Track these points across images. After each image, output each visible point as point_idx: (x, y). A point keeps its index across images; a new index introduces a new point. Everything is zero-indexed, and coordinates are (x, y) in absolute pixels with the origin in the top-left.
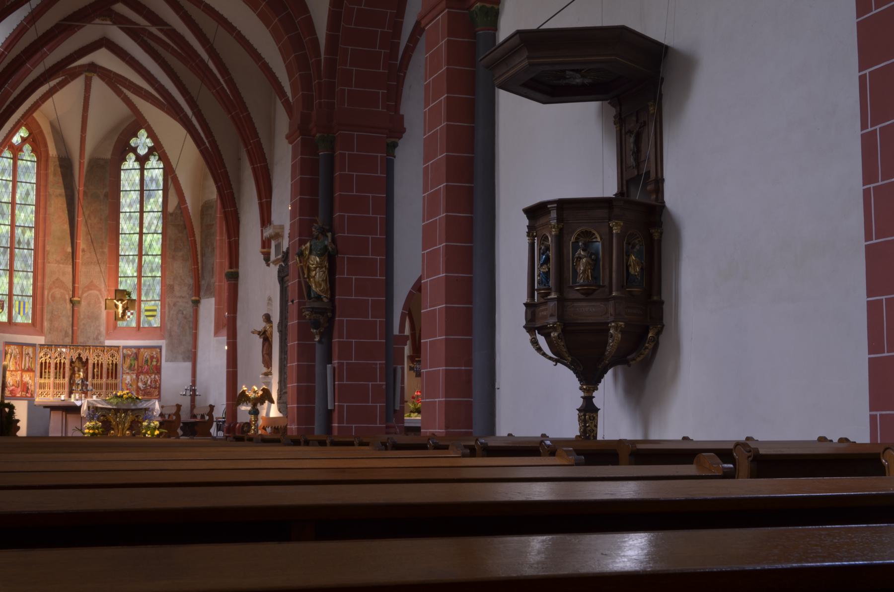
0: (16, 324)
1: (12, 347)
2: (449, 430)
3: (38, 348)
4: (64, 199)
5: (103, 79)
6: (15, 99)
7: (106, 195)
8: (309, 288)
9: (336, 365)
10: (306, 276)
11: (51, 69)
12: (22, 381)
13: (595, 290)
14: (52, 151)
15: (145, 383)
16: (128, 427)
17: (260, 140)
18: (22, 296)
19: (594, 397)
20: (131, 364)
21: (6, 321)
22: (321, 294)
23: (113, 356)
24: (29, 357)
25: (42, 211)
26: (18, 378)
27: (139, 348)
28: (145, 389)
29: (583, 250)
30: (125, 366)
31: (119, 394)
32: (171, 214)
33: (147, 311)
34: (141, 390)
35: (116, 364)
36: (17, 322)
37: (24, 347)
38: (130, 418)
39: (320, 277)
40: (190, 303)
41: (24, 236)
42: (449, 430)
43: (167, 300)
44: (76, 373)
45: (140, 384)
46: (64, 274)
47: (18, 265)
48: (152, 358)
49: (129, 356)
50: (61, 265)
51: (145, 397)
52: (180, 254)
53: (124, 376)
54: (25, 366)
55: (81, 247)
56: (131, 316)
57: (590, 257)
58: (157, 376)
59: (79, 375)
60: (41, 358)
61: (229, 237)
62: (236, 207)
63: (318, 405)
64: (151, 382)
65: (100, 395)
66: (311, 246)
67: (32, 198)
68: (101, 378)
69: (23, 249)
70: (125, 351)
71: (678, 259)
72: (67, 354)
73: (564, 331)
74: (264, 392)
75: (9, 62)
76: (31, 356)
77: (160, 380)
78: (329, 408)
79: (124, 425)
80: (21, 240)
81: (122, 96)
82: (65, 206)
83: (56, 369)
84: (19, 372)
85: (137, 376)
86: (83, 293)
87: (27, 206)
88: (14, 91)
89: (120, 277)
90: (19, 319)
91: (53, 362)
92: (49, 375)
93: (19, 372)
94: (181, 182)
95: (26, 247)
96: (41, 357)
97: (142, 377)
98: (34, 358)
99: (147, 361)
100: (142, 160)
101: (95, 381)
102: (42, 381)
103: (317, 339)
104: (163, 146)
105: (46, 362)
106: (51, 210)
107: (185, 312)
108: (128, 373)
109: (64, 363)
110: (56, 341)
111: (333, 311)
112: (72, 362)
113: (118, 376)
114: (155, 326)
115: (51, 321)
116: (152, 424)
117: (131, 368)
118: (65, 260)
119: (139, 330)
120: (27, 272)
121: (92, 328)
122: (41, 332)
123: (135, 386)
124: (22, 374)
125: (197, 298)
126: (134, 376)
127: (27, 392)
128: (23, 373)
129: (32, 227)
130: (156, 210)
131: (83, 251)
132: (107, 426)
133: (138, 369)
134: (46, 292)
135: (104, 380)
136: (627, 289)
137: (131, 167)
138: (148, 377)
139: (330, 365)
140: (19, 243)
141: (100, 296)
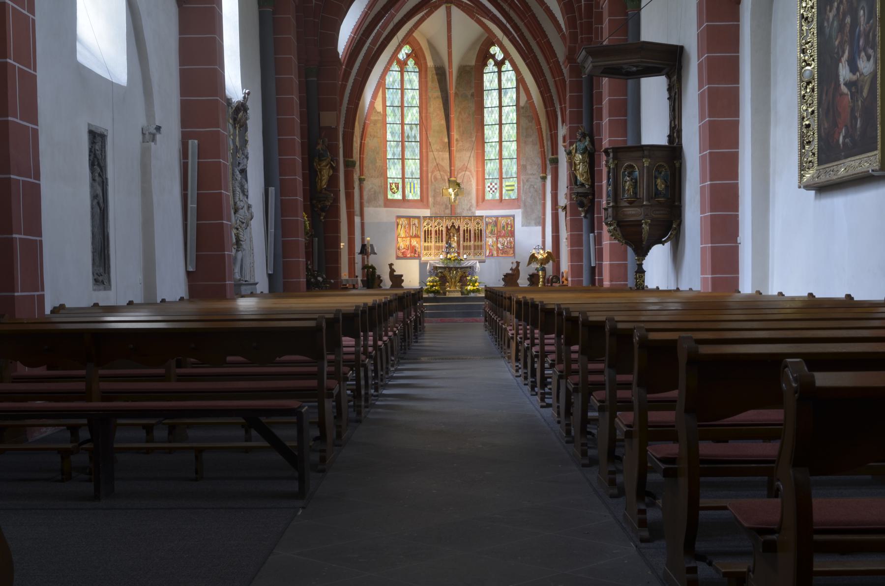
0: (409, 201)
1: (402, 219)
2: (613, 283)
3: (422, 221)
4: (441, 100)
5: (459, 8)
6: (387, 36)
7: (472, 95)
8: (576, 177)
9: (596, 234)
10: (573, 169)
11: (408, 13)
12: (411, 245)
13: (634, 201)
14: (430, 63)
15: (503, 245)
16: (459, 280)
17: (558, 60)
18: (412, 178)
19: (504, 275)
20: (492, 230)
21: (401, 199)
22: (583, 182)
23: (478, 223)
24: (416, 226)
25: (424, 111)
26: (408, 243)
27: (497, 217)
28: (503, 249)
29: (629, 177)
30: (488, 231)
31: (448, 257)
32: (523, 108)
33: (507, 186)
34: (500, 250)
35: (481, 230)
36: (409, 199)
37: (411, 219)
38: (460, 274)
39: (583, 170)
40: (539, 179)
41: (411, 131)
42: (613, 283)
43: (522, 177)
44: (452, 237)
45: (499, 245)
46: (443, 159)
47: (408, 154)
48: (507, 224)
49: (490, 223)
50: (440, 153)
51: (503, 255)
52: (531, 140)
53: (487, 240)
54: (413, 234)
55: (455, 138)
56: (495, 191)
57: (632, 180)
58: (511, 239)
59: (454, 239)
60: (425, 227)
61: (551, 131)
62: (554, 106)
63: (585, 263)
64: (507, 244)
65: (469, 254)
66: (576, 146)
67: (416, 102)
68: (470, 241)
69: (412, 142)
70: (487, 220)
71: (685, 180)
72: (446, 223)
73: (618, 225)
74: (548, 254)
75: (372, 17)
76: (417, 226)
77: (514, 241)
78: (592, 265)
79: (456, 279)
80: (410, 135)
81: (475, 19)
82: (442, 105)
83: (436, 234)
84: (409, 238)
85: (497, 239)
86: (457, 175)
87: (413, 108)
88: (384, 32)
89: (486, 160)
90: (410, 196)
91: (433, 230)
92: (431, 240)
93: (409, 238)
94: (527, 82)
95: (414, 140)
96: (425, 226)
97: (500, 239)
98: (419, 227)
99: (504, 227)
100: (499, 64)
101: (465, 244)
102: (426, 244)
103: (583, 215)
104: (511, 54)
105: (428, 230)
106: (431, 109)
107: (535, 187)
108: (490, 237)
109: (442, 231)
110: (438, 212)
111: (593, 195)
112: (448, 230)
113: (483, 239)
114: (514, 198)
115: (434, 197)
116: (473, 278)
117: (492, 232)
118: (443, 149)
119: (501, 201)
120: (415, 159)
121: (466, 201)
122: (427, 206)
123: (495, 247)
124: (410, 240)
125: (544, 175)
126: (495, 239)
127: (415, 253)
128: (412, 239)
129: (418, 124)
130: (511, 104)
131: (457, 140)
132: (443, 280)
133: (497, 234)
134: (430, 175)
135: (472, 242)
136: (656, 199)
137: (491, 70)
138: (505, 239)
139: (592, 234)
140: (408, 137)
141: (471, 176)
